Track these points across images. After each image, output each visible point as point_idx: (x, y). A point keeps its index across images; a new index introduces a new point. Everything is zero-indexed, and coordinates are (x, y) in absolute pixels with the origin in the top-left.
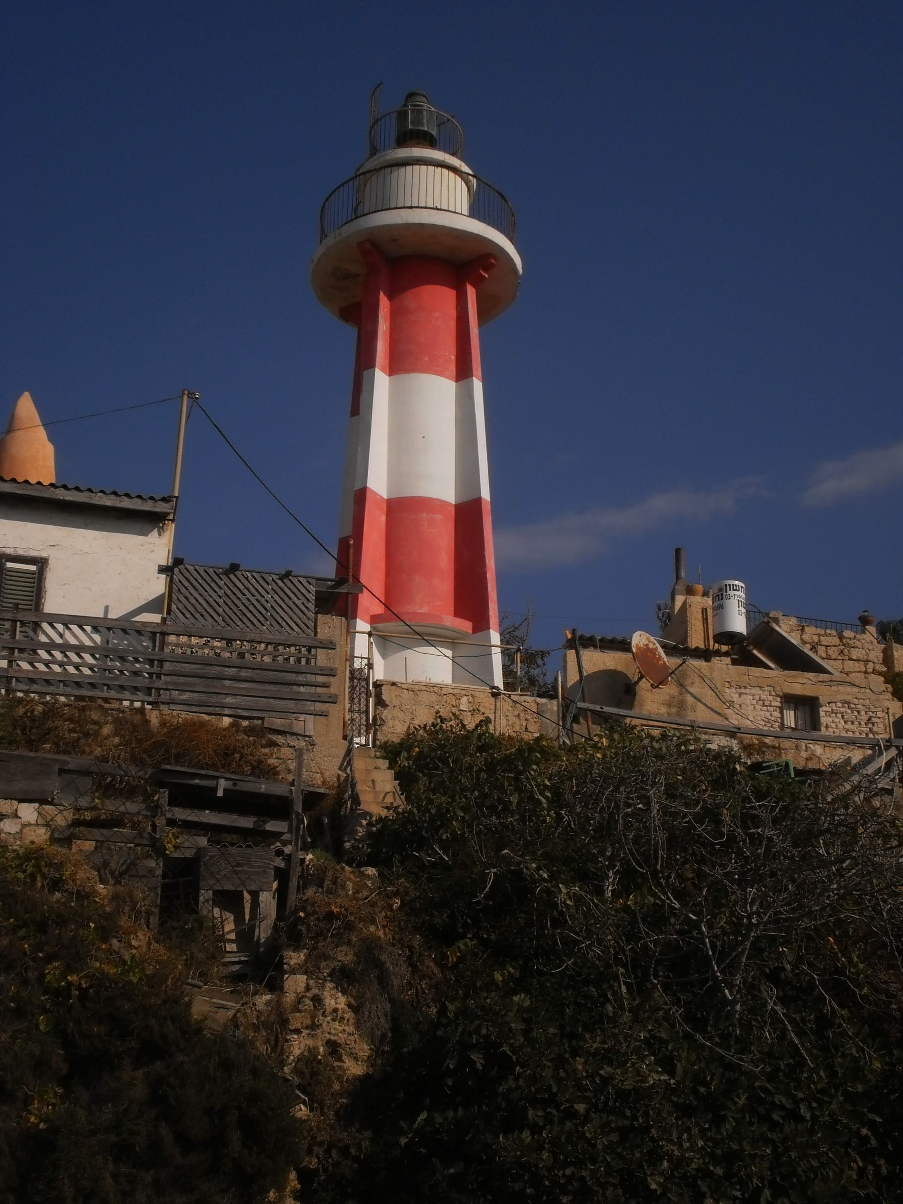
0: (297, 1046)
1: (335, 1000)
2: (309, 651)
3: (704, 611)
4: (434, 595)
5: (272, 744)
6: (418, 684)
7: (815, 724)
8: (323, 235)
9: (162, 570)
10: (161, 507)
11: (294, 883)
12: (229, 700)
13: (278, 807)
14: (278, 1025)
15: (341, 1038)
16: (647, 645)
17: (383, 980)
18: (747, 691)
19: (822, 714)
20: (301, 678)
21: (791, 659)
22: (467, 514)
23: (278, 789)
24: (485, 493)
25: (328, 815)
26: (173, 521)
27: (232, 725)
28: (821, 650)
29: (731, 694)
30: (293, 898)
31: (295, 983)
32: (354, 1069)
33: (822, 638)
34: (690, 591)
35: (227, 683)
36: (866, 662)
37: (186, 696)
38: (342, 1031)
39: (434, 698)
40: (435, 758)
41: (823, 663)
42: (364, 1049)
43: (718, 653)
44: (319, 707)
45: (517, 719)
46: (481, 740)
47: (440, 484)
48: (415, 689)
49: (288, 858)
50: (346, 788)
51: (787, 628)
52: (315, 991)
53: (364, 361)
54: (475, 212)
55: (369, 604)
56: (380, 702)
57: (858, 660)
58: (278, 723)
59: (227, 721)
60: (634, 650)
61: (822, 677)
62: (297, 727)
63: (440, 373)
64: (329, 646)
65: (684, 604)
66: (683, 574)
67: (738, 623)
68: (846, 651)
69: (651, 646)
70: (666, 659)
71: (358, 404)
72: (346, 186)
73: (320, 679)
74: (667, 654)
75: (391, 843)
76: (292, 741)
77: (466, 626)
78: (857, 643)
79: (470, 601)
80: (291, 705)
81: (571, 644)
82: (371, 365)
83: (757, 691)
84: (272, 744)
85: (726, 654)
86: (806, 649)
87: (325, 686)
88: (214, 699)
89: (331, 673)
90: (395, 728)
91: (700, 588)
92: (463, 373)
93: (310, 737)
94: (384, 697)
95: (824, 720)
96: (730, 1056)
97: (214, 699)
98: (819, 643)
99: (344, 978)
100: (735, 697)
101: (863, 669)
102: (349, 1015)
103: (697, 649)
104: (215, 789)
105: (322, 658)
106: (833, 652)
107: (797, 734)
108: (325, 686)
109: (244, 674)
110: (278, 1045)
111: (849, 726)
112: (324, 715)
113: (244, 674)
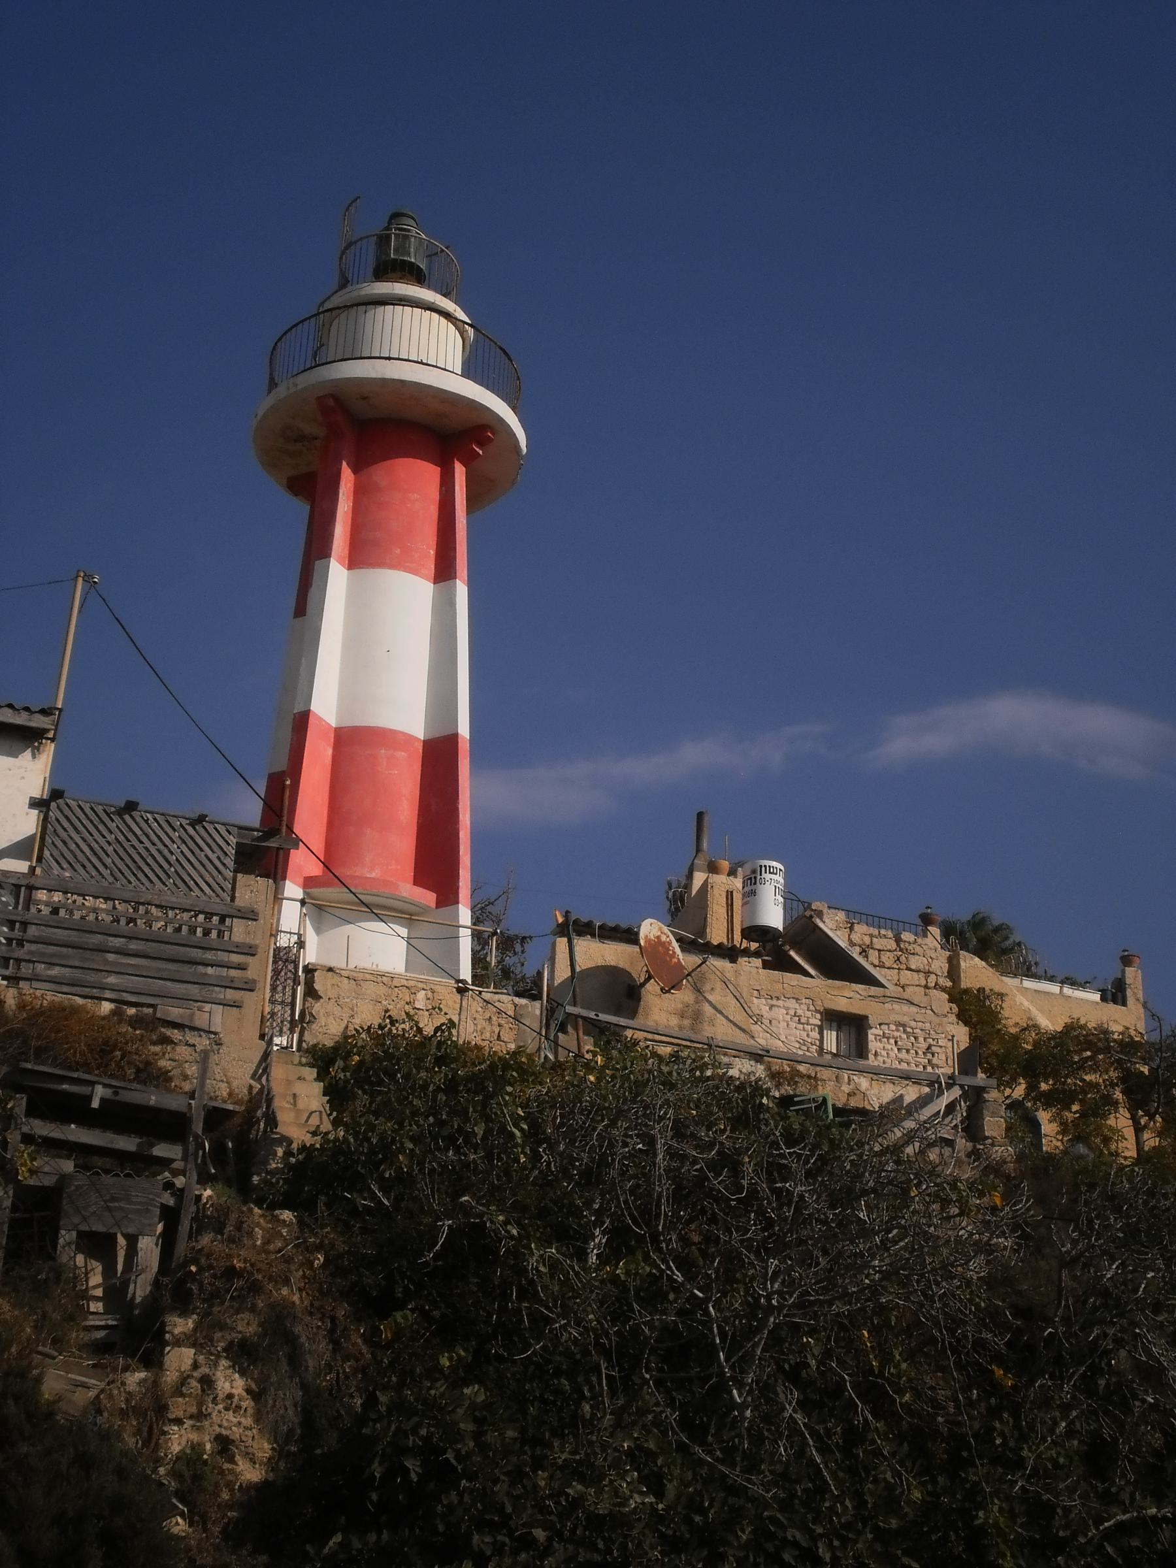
0: (177, 1440)
1: (231, 1383)
2: (223, 919)
3: (730, 895)
4: (388, 856)
5: (166, 1041)
6: (363, 971)
7: (860, 1049)
8: (273, 384)
9: (35, 803)
10: (38, 722)
11: (185, 1226)
12: (112, 979)
13: (171, 1126)
14: (153, 1412)
15: (236, 1433)
16: (658, 937)
17: (295, 1360)
18: (780, 1003)
19: (871, 1037)
20: (209, 956)
21: (838, 965)
22: (439, 755)
23: (174, 1103)
24: (464, 729)
25: (236, 1138)
26: (52, 740)
27: (114, 1013)
28: (873, 955)
29: (760, 1005)
30: (182, 1248)
31: (179, 1359)
32: (250, 1473)
33: (875, 940)
34: (713, 868)
35: (111, 957)
36: (928, 973)
37: (55, 971)
38: (237, 1424)
39: (382, 990)
40: (378, 1071)
41: (875, 972)
42: (264, 1448)
43: (746, 953)
44: (230, 994)
45: (489, 1024)
46: (441, 1050)
47: (406, 713)
48: (356, 978)
49: (179, 1194)
50: (260, 1103)
51: (832, 925)
52: (205, 1370)
53: (317, 547)
54: (469, 371)
55: (303, 862)
56: (311, 993)
57: (918, 971)
58: (175, 1013)
59: (107, 1007)
60: (642, 942)
61: (874, 990)
62: (200, 1020)
63: (415, 572)
64: (250, 915)
65: (705, 884)
66: (705, 845)
67: (773, 915)
68: (903, 959)
69: (664, 938)
70: (681, 957)
71: (304, 601)
72: (306, 323)
73: (235, 958)
74: (683, 950)
75: (316, 1180)
76: (191, 1037)
77: (428, 898)
78: (918, 949)
79: (435, 865)
80: (194, 990)
81: (563, 930)
82: (325, 554)
83: (792, 1004)
84: (166, 1041)
85: (757, 954)
86: (855, 953)
87: (242, 967)
88: (92, 977)
89: (250, 951)
90: (329, 1027)
91: (725, 865)
92: (444, 572)
93: (215, 1033)
94: (317, 986)
95: (873, 1045)
96: (735, 1475)
97: (92, 977)
98: (871, 946)
99: (243, 1355)
100: (765, 1009)
101: (923, 982)
102: (248, 1403)
103: (720, 945)
104: (89, 1098)
105: (239, 931)
106: (888, 958)
107: (840, 1062)
108: (242, 967)
109: (134, 946)
110: (152, 1438)
111: (903, 1055)
112: (237, 1005)
113: (134, 946)
